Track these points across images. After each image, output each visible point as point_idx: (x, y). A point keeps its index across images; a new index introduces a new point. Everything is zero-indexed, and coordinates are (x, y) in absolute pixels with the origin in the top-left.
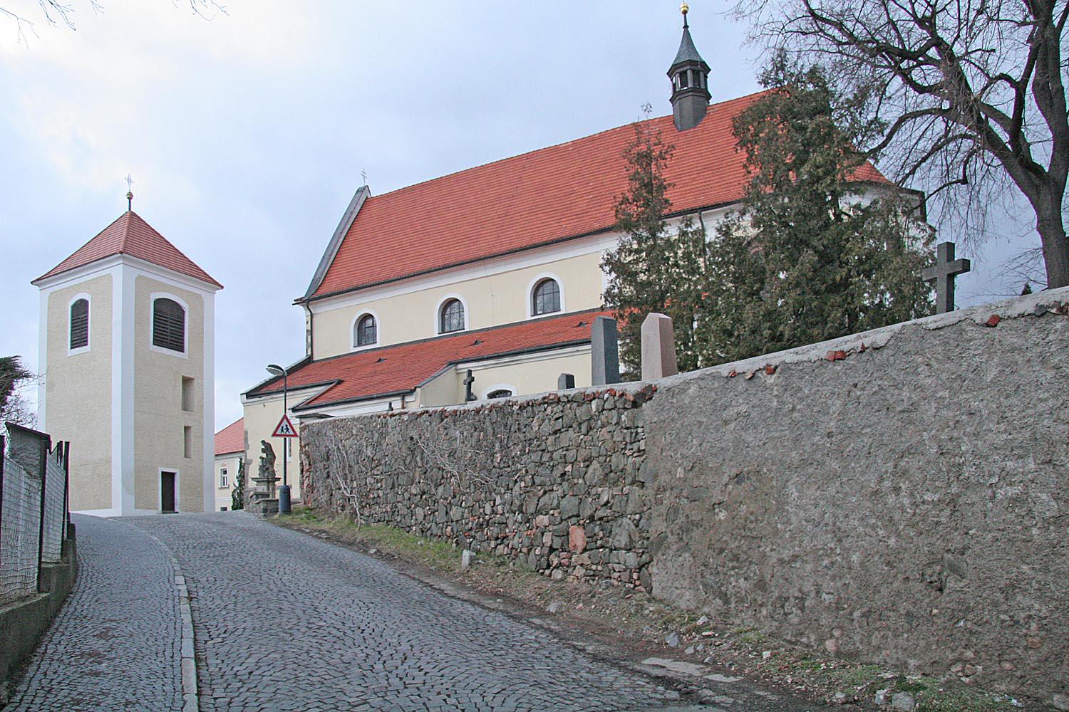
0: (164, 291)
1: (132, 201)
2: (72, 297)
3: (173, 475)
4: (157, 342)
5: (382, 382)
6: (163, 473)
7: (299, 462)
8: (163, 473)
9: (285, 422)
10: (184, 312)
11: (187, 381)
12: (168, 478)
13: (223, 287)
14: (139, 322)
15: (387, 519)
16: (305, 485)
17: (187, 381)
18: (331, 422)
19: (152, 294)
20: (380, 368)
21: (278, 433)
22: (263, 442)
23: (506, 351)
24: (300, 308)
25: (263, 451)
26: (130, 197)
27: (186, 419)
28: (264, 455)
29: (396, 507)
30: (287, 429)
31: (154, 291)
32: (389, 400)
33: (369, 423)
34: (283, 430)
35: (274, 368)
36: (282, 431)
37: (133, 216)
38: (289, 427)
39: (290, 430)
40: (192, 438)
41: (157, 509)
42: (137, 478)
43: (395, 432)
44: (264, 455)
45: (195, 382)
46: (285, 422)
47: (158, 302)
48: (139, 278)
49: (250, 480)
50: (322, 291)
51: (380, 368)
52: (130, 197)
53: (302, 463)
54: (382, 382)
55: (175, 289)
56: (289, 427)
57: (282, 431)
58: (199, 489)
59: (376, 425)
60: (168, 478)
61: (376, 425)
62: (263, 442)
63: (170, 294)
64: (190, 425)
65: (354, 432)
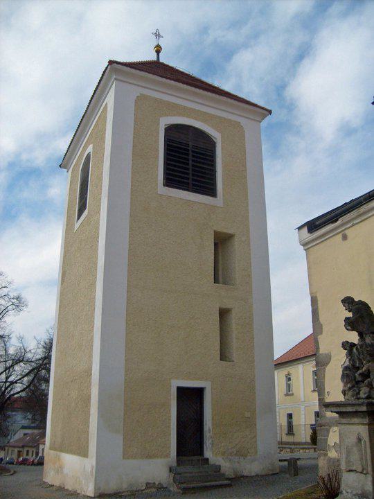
0: (180, 115)
3: (199, 392)
4: (172, 179)
11: (222, 242)
12: (190, 399)
13: (270, 112)
17: (222, 242)
22: (348, 302)
25: (351, 324)
27: (221, 297)
28: (354, 337)
31: (177, 378)
35: (314, 391)
40: (234, 326)
41: (168, 456)
42: (128, 412)
44: (354, 337)
45: (237, 244)
47: (170, 129)
48: (141, 99)
58: (248, 414)
60: (190, 399)
62: (348, 302)
64: (228, 307)
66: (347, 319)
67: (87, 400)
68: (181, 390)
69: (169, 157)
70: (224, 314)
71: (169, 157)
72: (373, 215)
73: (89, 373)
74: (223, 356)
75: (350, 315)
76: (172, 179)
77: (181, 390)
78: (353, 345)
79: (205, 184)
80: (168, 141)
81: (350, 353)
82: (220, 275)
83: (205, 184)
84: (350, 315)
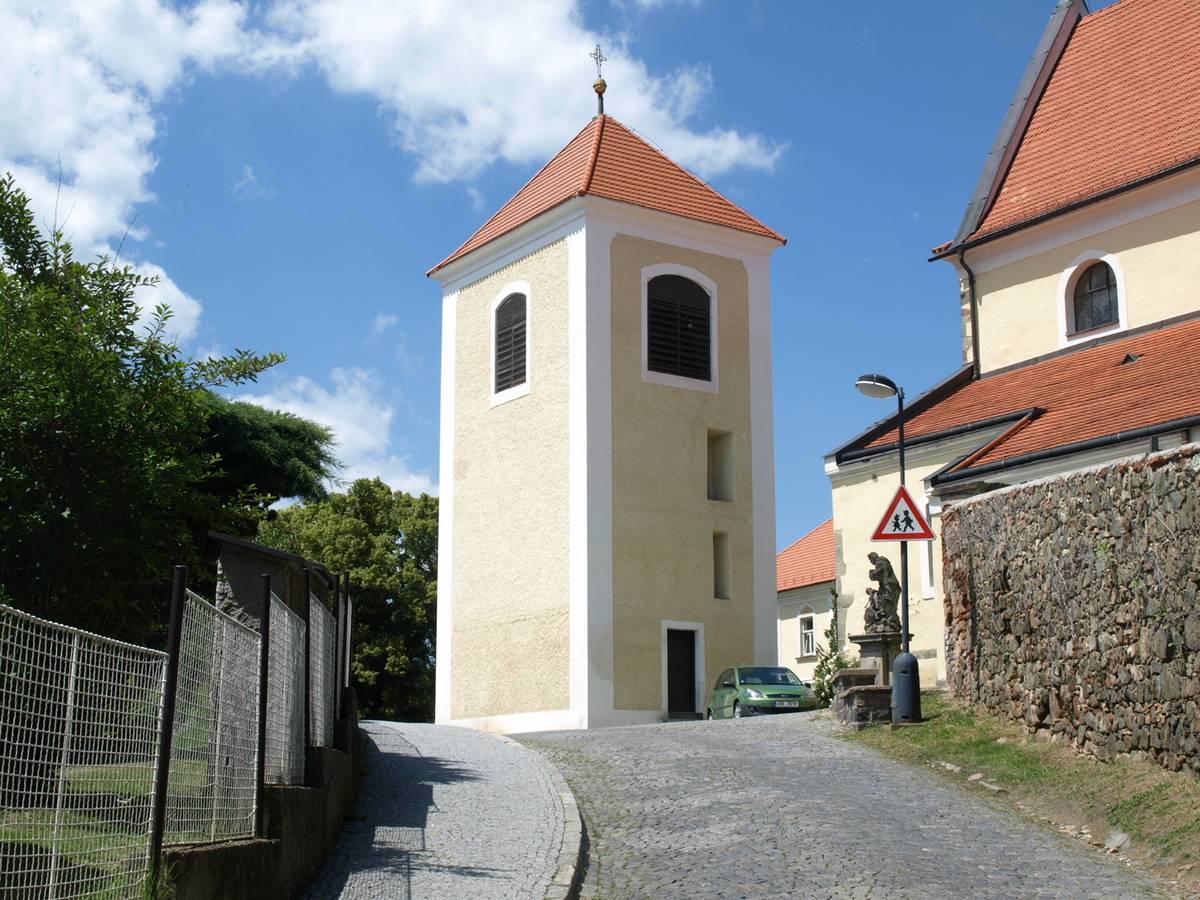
1: (604, 95)
2: (497, 292)
4: (658, 362)
5: (1135, 405)
6: (670, 632)
7: (944, 596)
8: (670, 632)
9: (902, 506)
10: (708, 298)
11: (716, 441)
12: (682, 644)
14: (619, 327)
15: (1156, 743)
16: (957, 652)
17: (716, 441)
18: (1006, 497)
19: (644, 270)
20: (1129, 376)
21: (889, 529)
23: (1087, 437)
24: (947, 266)
25: (874, 576)
26: (600, 89)
29: (1180, 710)
30: (908, 521)
32: (1079, 242)
33: (1102, 488)
34: (900, 523)
36: (897, 525)
37: (606, 123)
38: (911, 515)
39: (915, 523)
41: (659, 708)
43: (1169, 507)
44: (876, 585)
45: (734, 442)
46: (902, 506)
47: (658, 285)
49: (848, 641)
50: (994, 222)
51: (1129, 376)
52: (600, 89)
53: (948, 601)
54: (1135, 405)
55: (687, 249)
56: (911, 515)
57: (897, 525)
59: (1118, 492)
60: (682, 644)
61: (1118, 492)
63: (679, 266)
65: (1063, 516)
66: (871, 571)
67: (562, 645)
68: (671, 633)
69: (654, 356)
70: (718, 538)
71: (654, 356)
72: (861, 379)
73: (564, 612)
74: (719, 594)
75: (873, 567)
76: (658, 362)
77: (671, 633)
78: (874, 592)
79: (699, 368)
80: (652, 301)
81: (872, 600)
82: (716, 491)
83: (699, 368)
84: (873, 567)
